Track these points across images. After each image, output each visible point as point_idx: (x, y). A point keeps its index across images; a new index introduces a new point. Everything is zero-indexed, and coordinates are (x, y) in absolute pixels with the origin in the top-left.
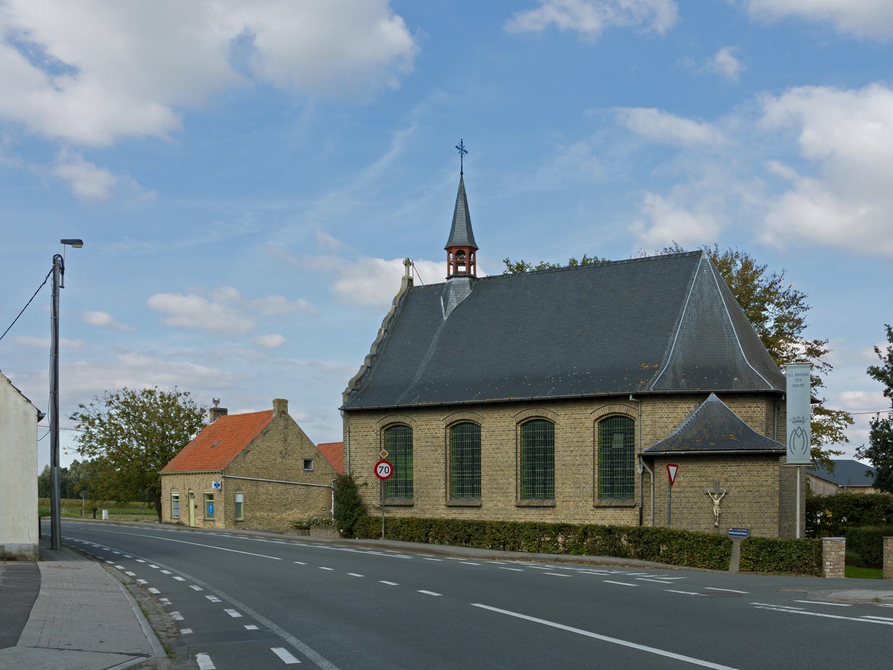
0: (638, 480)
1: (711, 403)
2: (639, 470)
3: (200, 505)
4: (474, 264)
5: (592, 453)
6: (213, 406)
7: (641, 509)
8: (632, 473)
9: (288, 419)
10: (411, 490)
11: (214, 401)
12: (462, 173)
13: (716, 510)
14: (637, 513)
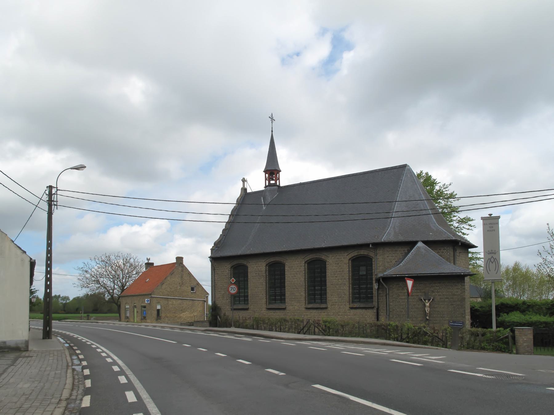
0: (375, 293)
1: (419, 248)
2: (375, 286)
3: (140, 311)
4: (279, 179)
5: (348, 278)
6: (147, 262)
7: (378, 309)
8: (372, 288)
9: (184, 266)
10: (248, 300)
11: (147, 259)
12: (272, 131)
13: (427, 310)
14: (375, 311)
